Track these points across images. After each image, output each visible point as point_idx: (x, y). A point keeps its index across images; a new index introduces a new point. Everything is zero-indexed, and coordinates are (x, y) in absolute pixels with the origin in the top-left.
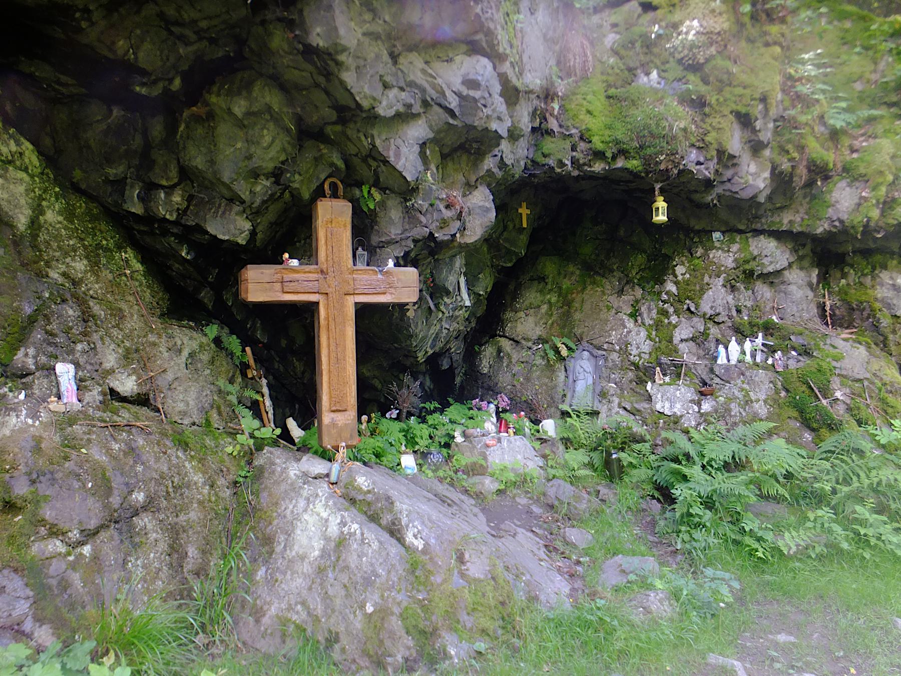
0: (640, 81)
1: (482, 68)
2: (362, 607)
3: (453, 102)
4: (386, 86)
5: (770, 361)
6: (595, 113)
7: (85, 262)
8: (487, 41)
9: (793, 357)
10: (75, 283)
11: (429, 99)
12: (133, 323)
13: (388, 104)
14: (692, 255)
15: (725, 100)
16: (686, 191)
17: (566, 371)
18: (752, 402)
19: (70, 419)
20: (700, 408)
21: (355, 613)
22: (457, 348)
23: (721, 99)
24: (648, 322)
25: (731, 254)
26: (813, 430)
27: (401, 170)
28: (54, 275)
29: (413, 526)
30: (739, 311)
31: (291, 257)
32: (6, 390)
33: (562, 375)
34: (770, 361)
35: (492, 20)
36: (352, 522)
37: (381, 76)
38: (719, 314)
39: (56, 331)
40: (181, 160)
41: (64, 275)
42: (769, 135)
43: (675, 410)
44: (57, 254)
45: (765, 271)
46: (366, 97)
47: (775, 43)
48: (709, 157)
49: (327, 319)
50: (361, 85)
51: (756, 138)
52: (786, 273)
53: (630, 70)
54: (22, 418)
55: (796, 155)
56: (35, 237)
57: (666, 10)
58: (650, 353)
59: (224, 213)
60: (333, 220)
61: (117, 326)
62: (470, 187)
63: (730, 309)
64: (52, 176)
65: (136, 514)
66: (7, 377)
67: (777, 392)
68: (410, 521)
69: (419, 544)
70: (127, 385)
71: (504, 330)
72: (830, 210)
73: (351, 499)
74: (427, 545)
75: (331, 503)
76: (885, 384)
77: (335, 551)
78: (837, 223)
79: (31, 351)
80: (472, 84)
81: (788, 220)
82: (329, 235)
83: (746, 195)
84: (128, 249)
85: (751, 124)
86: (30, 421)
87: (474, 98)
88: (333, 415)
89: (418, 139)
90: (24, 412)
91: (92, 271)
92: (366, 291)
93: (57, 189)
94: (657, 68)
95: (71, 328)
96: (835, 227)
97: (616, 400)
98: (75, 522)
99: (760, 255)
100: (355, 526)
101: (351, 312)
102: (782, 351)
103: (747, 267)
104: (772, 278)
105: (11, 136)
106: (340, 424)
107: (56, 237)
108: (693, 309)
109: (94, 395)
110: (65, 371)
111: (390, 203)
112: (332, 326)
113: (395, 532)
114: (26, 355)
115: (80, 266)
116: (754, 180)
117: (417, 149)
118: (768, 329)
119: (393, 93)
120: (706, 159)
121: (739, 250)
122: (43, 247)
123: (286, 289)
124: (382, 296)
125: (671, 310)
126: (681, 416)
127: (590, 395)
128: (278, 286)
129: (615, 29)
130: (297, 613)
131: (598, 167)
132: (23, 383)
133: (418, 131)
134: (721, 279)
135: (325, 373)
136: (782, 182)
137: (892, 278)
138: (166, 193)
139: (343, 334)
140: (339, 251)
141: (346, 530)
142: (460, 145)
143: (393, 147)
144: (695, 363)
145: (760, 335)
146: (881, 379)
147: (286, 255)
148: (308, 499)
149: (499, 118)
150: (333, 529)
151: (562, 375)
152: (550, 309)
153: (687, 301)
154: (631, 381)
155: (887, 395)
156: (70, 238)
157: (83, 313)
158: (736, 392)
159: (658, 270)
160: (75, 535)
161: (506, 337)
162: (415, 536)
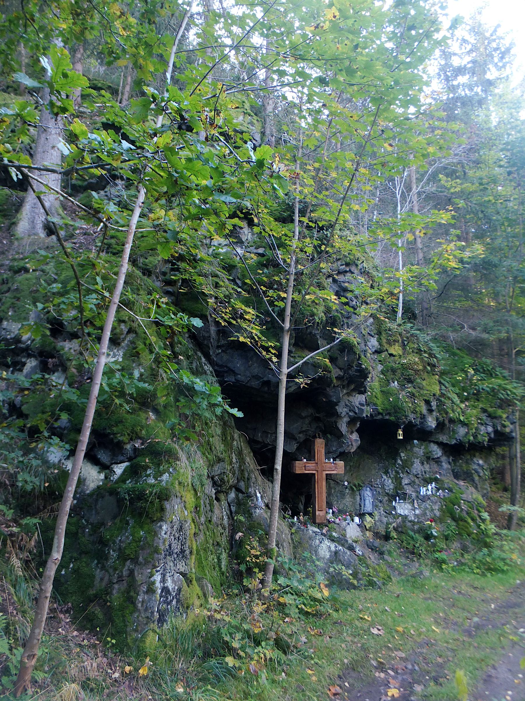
33: (358, 498)
60: (320, 445)
69: (361, 553)
81: (443, 438)
83: (429, 429)
101: (324, 476)
104: (437, 461)
118: (436, 480)
131: (380, 417)
136: (441, 426)
150: (333, 548)
159: (394, 454)
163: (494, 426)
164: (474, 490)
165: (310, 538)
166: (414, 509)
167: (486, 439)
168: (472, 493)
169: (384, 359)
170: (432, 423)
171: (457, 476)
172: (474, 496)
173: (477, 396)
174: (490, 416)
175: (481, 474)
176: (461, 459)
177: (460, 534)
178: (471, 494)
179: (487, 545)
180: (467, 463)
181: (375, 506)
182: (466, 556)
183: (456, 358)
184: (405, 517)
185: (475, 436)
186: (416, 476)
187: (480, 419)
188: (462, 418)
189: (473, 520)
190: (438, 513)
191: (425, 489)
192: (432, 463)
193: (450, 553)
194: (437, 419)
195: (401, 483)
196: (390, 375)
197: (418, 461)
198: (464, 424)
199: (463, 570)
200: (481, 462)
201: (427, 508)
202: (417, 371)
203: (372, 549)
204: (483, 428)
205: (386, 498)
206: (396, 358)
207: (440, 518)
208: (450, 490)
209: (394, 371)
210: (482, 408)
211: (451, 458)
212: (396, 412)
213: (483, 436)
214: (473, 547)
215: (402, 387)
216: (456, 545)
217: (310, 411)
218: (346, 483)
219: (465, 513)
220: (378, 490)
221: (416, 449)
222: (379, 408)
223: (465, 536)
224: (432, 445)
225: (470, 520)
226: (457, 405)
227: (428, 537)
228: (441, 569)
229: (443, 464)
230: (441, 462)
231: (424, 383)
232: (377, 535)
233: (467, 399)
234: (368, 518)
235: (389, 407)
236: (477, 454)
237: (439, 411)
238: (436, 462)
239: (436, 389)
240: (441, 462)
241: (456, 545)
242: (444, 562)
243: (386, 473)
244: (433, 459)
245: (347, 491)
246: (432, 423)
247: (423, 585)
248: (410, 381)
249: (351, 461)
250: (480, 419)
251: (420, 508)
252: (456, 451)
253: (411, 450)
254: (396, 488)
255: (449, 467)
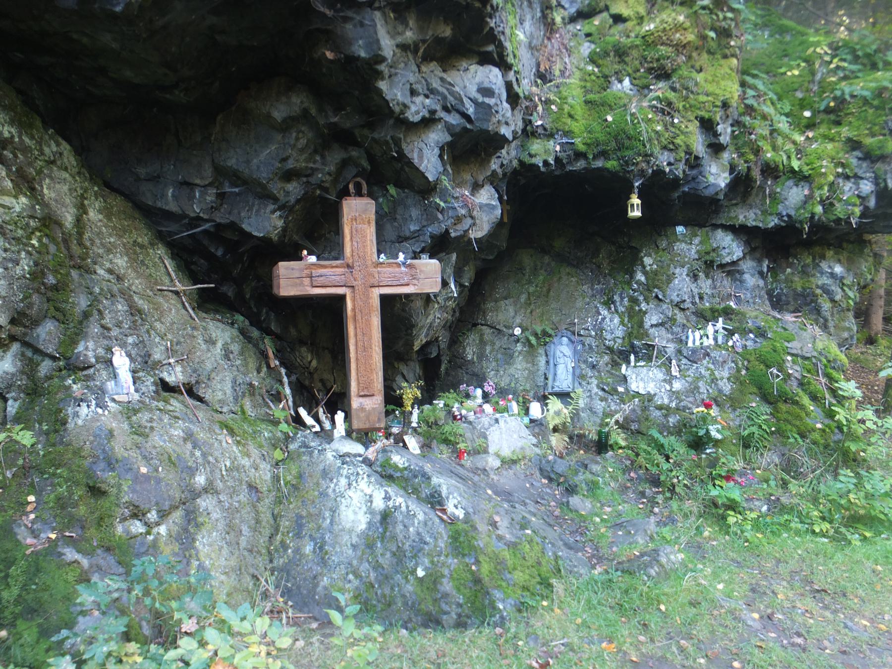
0: (615, 87)
1: (493, 76)
2: (413, 572)
3: (471, 110)
4: (413, 93)
5: (730, 343)
6: (576, 117)
7: (126, 259)
8: (497, 52)
9: (750, 338)
10: (119, 278)
11: (449, 105)
12: (328, 446)
13: (417, 109)
14: (658, 247)
15: (691, 107)
16: (658, 188)
17: (547, 355)
18: (717, 380)
19: (129, 410)
20: (672, 387)
21: (406, 577)
22: (444, 339)
23: (688, 106)
24: (621, 309)
25: (694, 247)
26: (770, 403)
27: (424, 171)
28: (101, 272)
29: (454, 497)
30: (701, 298)
31: (309, 254)
32: (70, 382)
33: (542, 360)
34: (730, 343)
35: (503, 33)
36: (396, 496)
37: (411, 84)
38: (685, 301)
39: (110, 325)
40: (216, 161)
41: (110, 271)
42: (728, 138)
43: (648, 389)
44: (101, 251)
45: (724, 262)
46: (398, 104)
47: (733, 56)
48: (678, 158)
49: (354, 310)
50: (393, 91)
51: (717, 142)
52: (741, 263)
53: (606, 77)
54: (93, 407)
55: (752, 157)
56: (80, 234)
57: (635, 22)
58: (623, 338)
59: (258, 211)
60: (358, 215)
61: (159, 320)
62: (476, 187)
63: (693, 297)
64: (87, 175)
65: (199, 495)
66: (69, 370)
67: (739, 371)
68: (449, 493)
69: (460, 513)
70: (175, 376)
71: (485, 318)
72: (779, 207)
73: (387, 474)
74: (467, 514)
75: (373, 479)
76: (829, 361)
77: (381, 524)
78: (786, 218)
79: (91, 344)
80: (487, 92)
81: (748, 216)
82: (354, 232)
83: (708, 192)
84: (160, 245)
85: (713, 128)
86: (100, 411)
87: (489, 105)
88: (361, 400)
89: (438, 142)
90: (94, 402)
91: (131, 266)
92: (390, 283)
93: (96, 189)
94: (629, 75)
95: (121, 322)
96: (784, 221)
97: (595, 382)
98: (153, 503)
99: (718, 247)
100: (400, 500)
101: (376, 303)
102: (740, 334)
103: (708, 258)
104: (731, 270)
105: (51, 137)
106: (368, 408)
107: (98, 234)
108: (660, 297)
109: (149, 384)
110: (121, 361)
111: (409, 201)
112: (359, 317)
113: (435, 501)
114: (87, 349)
115: (121, 262)
116: (715, 179)
117: (437, 151)
118: (727, 313)
119: (419, 100)
120: (676, 160)
121: (701, 243)
122: (88, 244)
123: (315, 284)
124: (406, 287)
125: (641, 298)
126: (655, 395)
127: (570, 377)
128: (307, 281)
129: (589, 38)
130: (350, 581)
131: (580, 164)
132: (85, 376)
133: (436, 137)
134: (685, 269)
135: (353, 361)
137: (830, 267)
138: (200, 191)
139: (368, 323)
140: (364, 246)
141: (391, 504)
142: (471, 147)
143: (416, 150)
144: (684, 342)
145: (721, 319)
146: (826, 357)
147: (305, 252)
148: (348, 477)
149: (507, 123)
150: (379, 504)
151: (542, 360)
152: (529, 299)
153: (656, 290)
154: (607, 365)
155: (831, 371)
156: (111, 235)
157: (130, 307)
158: (703, 372)
159: (627, 261)
160: (152, 516)
161: (488, 325)
162: (456, 507)
163: (876, 181)
164: (818, 331)
165: (326, 474)
166: (670, 380)
167: (857, 211)
168: (814, 338)
169: (600, 29)
170: (717, 176)
171: (778, 303)
172: (820, 345)
173: (836, 113)
174: (869, 157)
175: (838, 297)
176: (790, 265)
177: (780, 433)
178: (809, 339)
179: (852, 461)
180: (804, 273)
181: (579, 377)
182: (794, 486)
183: (788, 38)
184: (650, 397)
185: (828, 205)
186: (678, 305)
187: (843, 165)
188: (795, 164)
189: (814, 398)
190: (727, 387)
191: (697, 334)
192: (719, 275)
193: (749, 483)
194: (732, 168)
195: (641, 324)
196: (611, 64)
197: (685, 271)
198: (799, 177)
199: (786, 526)
200: (838, 269)
201: (701, 377)
202: (680, 47)
203: (550, 480)
204: (848, 186)
205: (606, 358)
206: (629, 24)
207: (730, 398)
208: (761, 333)
209: (621, 53)
210: (849, 140)
211: (766, 263)
212: (620, 147)
213: (847, 203)
214: (813, 463)
215: (643, 89)
216: (770, 458)
217: (297, 102)
218: (517, 331)
219: (795, 384)
220: (588, 341)
221: (680, 247)
222: (577, 141)
223: (793, 438)
224: (720, 233)
225: (806, 401)
226: (786, 137)
227: (698, 444)
228: (725, 528)
229: (747, 276)
230: (741, 273)
231: (700, 77)
232: (577, 440)
233: (811, 125)
234: (555, 404)
235: (601, 137)
236: (830, 253)
237: (737, 149)
238: (729, 273)
239: (732, 90)
240: (741, 273)
241: (770, 458)
242: (732, 506)
243: (609, 303)
244: (722, 266)
245: (519, 347)
246: (717, 176)
247: (653, 602)
248: (663, 75)
249: (530, 282)
250: (843, 165)
251: (684, 377)
252: (780, 245)
253: (669, 249)
254: (629, 335)
255: (761, 283)
